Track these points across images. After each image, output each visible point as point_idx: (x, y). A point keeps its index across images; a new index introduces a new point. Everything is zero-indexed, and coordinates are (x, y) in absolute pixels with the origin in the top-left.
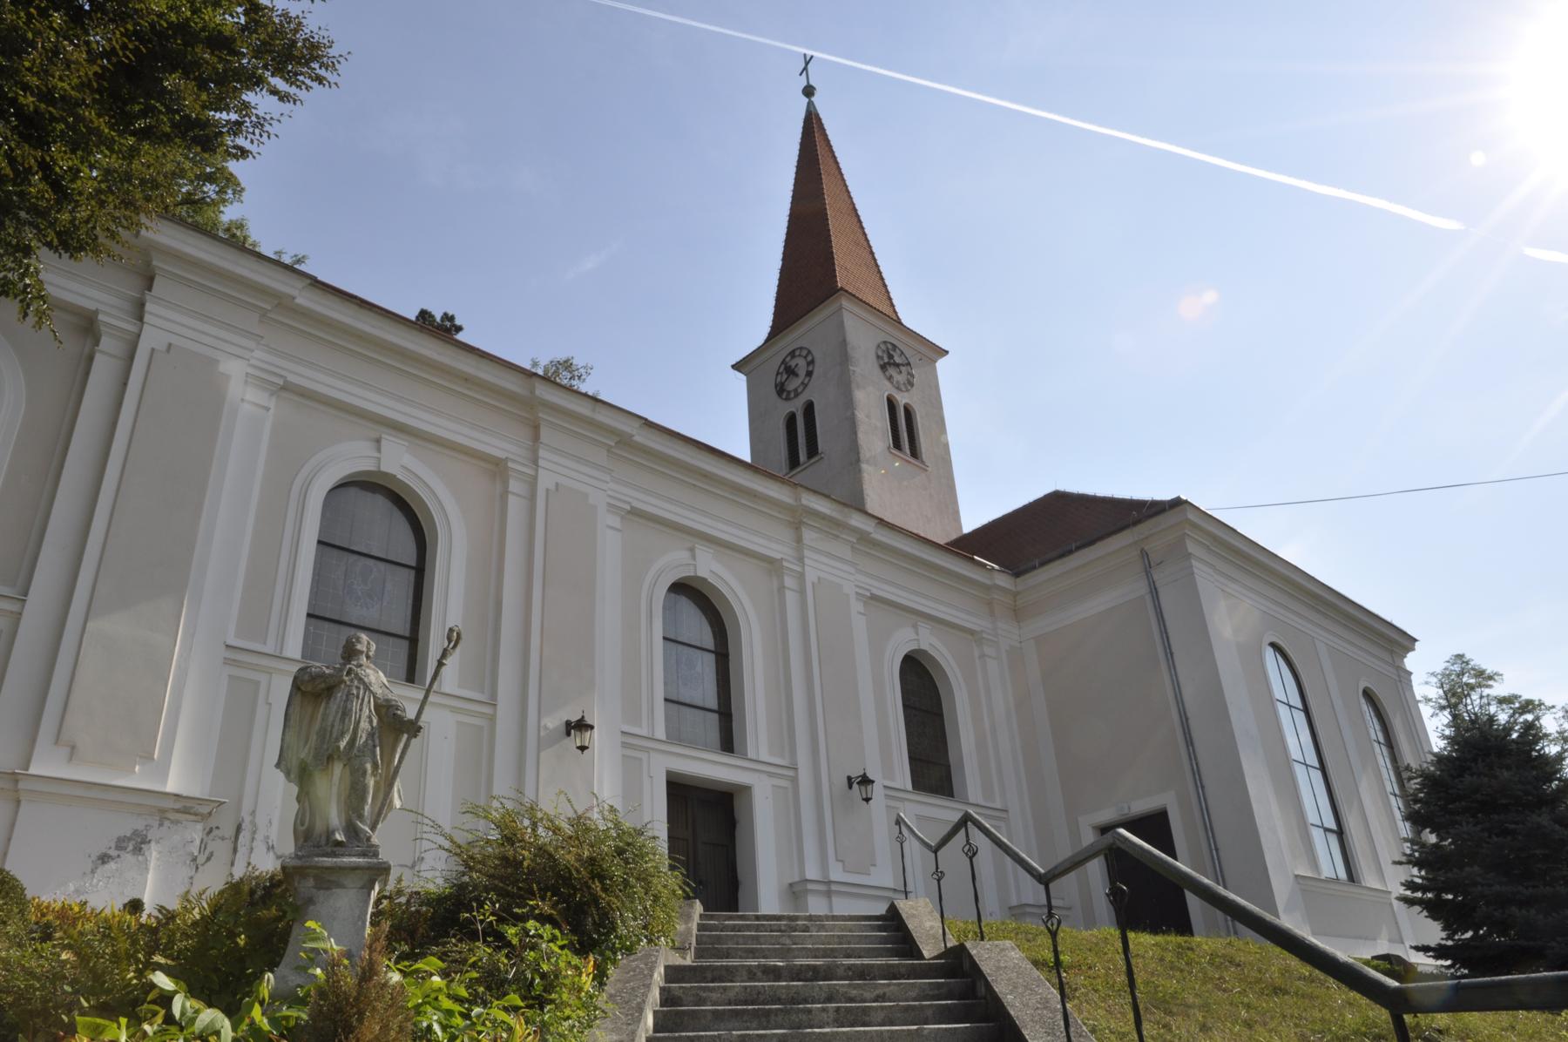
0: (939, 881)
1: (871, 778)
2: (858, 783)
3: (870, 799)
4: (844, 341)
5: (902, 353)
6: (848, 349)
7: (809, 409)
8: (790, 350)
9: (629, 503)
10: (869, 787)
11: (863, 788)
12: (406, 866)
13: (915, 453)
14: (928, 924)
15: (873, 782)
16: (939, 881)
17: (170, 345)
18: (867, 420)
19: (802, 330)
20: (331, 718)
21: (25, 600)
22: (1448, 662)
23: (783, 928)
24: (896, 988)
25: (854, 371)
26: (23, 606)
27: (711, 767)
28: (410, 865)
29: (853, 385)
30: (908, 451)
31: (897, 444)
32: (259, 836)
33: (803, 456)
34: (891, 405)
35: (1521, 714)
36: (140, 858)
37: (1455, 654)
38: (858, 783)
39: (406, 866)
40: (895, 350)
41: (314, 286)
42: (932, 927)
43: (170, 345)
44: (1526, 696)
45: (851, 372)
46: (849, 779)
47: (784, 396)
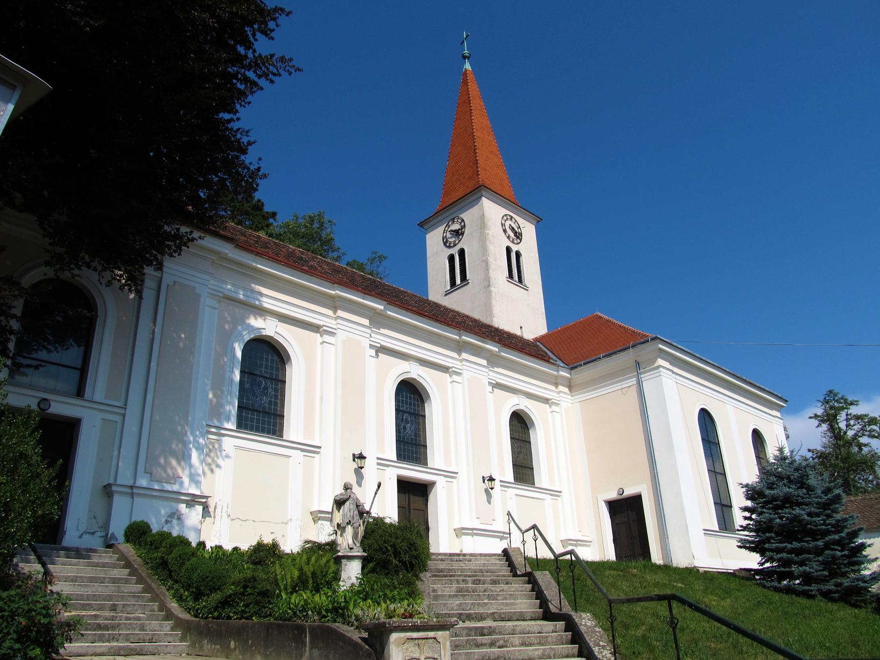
0: (524, 545)
1: (494, 477)
2: (487, 480)
3: (493, 488)
4: (483, 215)
5: (516, 220)
6: (485, 220)
7: (462, 253)
8: (452, 218)
9: (380, 343)
10: (493, 482)
11: (490, 482)
12: (284, 523)
13: (520, 280)
14: (519, 559)
15: (495, 480)
16: (524, 545)
17: (175, 282)
18: (494, 261)
19: (461, 205)
20: (346, 511)
21: (126, 408)
22: (826, 395)
23: (461, 559)
24: (507, 587)
25: (488, 234)
26: (125, 411)
27: (413, 472)
28: (286, 522)
29: (488, 242)
30: (517, 280)
31: (511, 276)
32: (224, 511)
33: (458, 281)
34: (509, 250)
35: (869, 425)
36: (180, 521)
37: (828, 390)
38: (487, 480)
39: (284, 523)
40: (513, 240)
41: (237, 247)
42: (520, 561)
43: (175, 282)
44: (872, 415)
45: (486, 234)
46: (483, 477)
47: (448, 245)
